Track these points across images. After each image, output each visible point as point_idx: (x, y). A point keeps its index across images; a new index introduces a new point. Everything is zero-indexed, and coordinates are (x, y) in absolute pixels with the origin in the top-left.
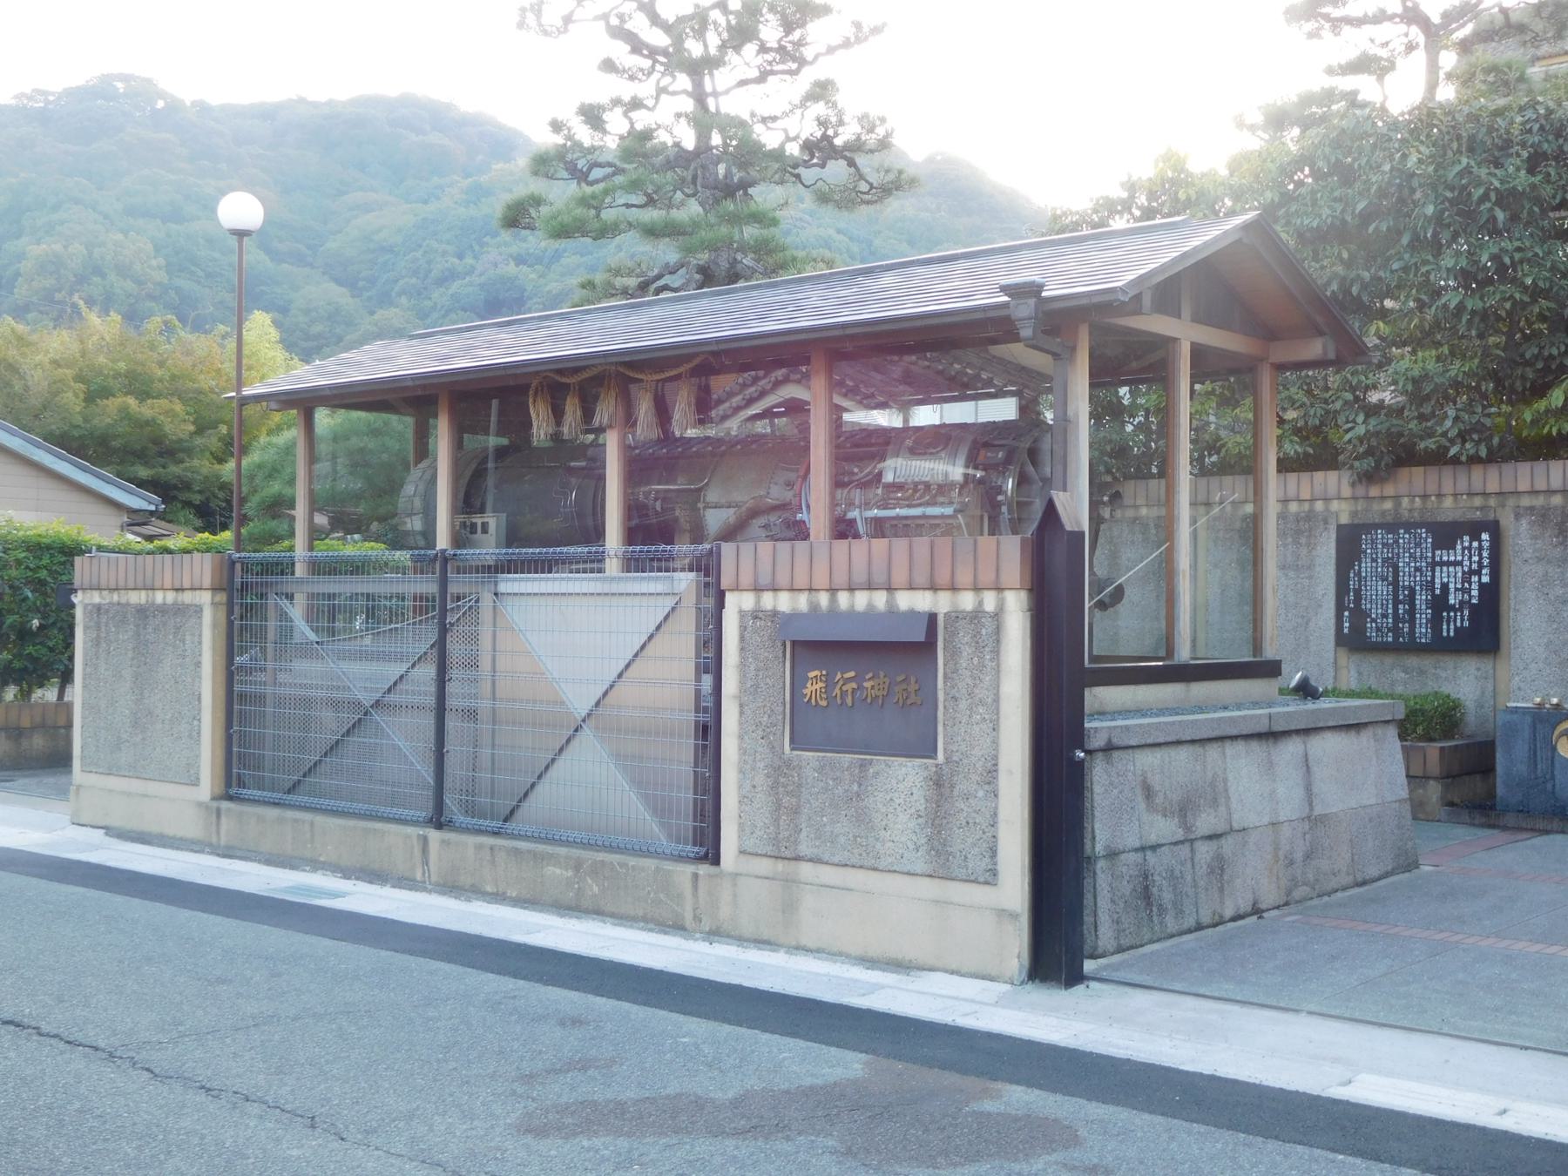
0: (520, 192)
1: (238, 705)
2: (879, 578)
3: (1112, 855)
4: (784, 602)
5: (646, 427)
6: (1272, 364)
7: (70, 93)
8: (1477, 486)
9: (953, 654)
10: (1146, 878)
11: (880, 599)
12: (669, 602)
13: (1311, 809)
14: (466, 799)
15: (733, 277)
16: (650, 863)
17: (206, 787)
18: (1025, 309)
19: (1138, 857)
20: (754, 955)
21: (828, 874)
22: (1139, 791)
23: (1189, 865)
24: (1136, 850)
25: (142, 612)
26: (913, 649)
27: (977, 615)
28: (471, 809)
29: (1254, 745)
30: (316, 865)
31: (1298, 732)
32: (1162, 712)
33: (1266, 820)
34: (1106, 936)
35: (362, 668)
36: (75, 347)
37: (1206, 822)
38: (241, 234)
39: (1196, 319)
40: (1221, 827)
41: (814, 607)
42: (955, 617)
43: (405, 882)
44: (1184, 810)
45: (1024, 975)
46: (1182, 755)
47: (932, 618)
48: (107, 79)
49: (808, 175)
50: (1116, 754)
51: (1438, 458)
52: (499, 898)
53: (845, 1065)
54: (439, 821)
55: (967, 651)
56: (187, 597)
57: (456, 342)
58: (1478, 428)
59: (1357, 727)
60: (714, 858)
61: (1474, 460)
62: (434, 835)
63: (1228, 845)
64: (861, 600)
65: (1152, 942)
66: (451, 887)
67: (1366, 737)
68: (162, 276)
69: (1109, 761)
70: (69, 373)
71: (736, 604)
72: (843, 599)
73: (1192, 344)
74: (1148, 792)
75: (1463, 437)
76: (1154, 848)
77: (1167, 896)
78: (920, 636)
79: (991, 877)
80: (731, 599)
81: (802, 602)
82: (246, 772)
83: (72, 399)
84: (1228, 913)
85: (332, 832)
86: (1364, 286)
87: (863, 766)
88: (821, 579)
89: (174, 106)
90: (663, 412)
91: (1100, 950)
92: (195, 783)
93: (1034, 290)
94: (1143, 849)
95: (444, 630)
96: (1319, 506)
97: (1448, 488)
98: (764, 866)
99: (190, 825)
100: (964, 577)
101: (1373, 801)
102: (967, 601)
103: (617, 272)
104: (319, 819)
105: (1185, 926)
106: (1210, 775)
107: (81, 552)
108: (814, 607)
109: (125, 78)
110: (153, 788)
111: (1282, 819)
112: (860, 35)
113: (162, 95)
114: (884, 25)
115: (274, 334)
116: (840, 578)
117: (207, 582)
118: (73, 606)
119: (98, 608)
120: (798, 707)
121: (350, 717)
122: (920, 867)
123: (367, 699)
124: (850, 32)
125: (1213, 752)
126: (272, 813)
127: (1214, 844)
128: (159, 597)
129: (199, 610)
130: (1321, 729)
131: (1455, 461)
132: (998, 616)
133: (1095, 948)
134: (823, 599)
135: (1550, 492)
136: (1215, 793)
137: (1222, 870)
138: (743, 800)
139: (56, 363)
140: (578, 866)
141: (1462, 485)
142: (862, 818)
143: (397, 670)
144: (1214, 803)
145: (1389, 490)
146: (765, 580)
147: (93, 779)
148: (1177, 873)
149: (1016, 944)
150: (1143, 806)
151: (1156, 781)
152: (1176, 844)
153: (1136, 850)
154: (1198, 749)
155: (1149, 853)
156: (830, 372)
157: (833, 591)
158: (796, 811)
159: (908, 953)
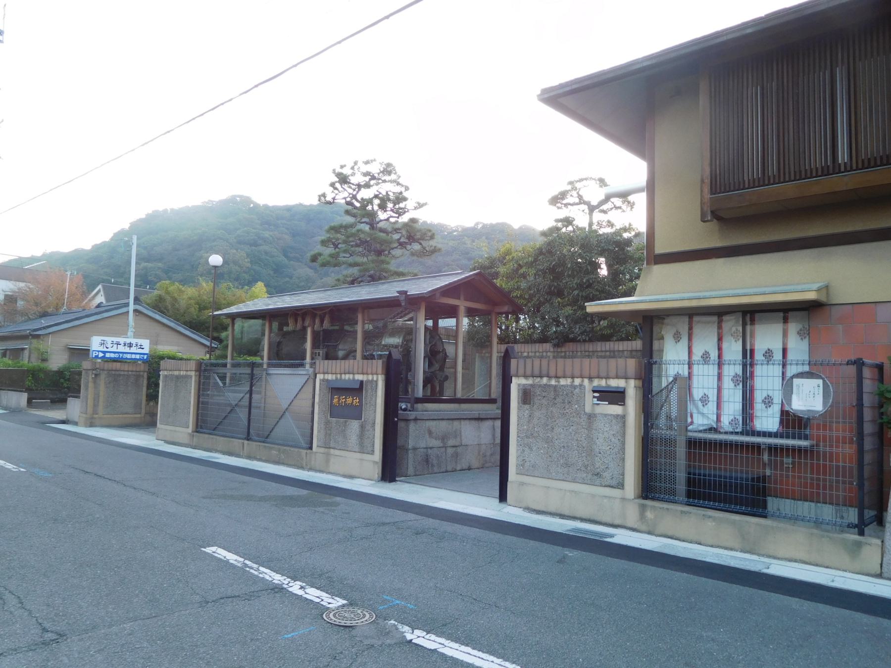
0: (316, 251)
1: (201, 405)
2: (603, 374)
3: (415, 449)
4: (330, 377)
5: (317, 326)
7: (221, 201)
8: (587, 349)
9: (367, 391)
11: (351, 376)
12: (307, 377)
14: (255, 431)
15: (380, 279)
16: (296, 450)
17: (190, 430)
18: (402, 298)
20: (311, 473)
21: (337, 452)
25: (178, 377)
26: (358, 390)
27: (372, 380)
28: (258, 435)
29: (473, 422)
30: (216, 451)
31: (491, 419)
34: (411, 470)
35: (234, 395)
36: (197, 293)
37: (451, 442)
38: (215, 267)
39: (466, 300)
41: (337, 378)
42: (368, 381)
43: (238, 456)
44: (444, 438)
46: (444, 423)
47: (362, 382)
48: (234, 197)
49: (409, 247)
51: (574, 340)
52: (260, 460)
53: (304, 492)
54: (248, 438)
55: (370, 391)
56: (189, 373)
57: (321, 295)
58: (585, 331)
60: (311, 448)
61: (585, 341)
62: (246, 442)
63: (459, 450)
64: (347, 377)
66: (249, 457)
68: (249, 265)
70: (192, 302)
71: (320, 377)
72: (343, 376)
74: (430, 433)
75: (582, 333)
76: (431, 448)
77: (435, 462)
78: (358, 387)
79: (372, 452)
81: (334, 377)
82: (201, 426)
83: (194, 311)
84: (458, 468)
85: (221, 441)
86: (555, 287)
87: (346, 422)
88: (338, 371)
89: (257, 206)
90: (322, 322)
92: (188, 427)
93: (405, 292)
95: (251, 386)
96: (545, 354)
97: (579, 349)
98: (322, 450)
99: (186, 440)
100: (369, 371)
102: (370, 377)
103: (347, 276)
104: (218, 438)
108: (337, 378)
109: (239, 196)
110: (178, 429)
112: (420, 206)
113: (252, 202)
114: (426, 204)
115: (265, 289)
116: (342, 371)
118: (159, 375)
119: (166, 376)
120: (332, 405)
121: (229, 409)
122: (357, 450)
123: (234, 403)
124: (416, 205)
125: (456, 423)
126: (207, 436)
127: (454, 449)
128: (182, 373)
129: (191, 377)
131: (579, 341)
132: (376, 382)
134: (339, 376)
135: (606, 351)
136: (457, 434)
138: (319, 432)
139: (190, 298)
140: (279, 450)
141: (583, 349)
142: (345, 437)
143: (242, 395)
144: (456, 437)
145: (563, 350)
146: (593, 374)
147: (163, 426)
149: (377, 471)
151: (433, 430)
154: (451, 422)
156: (363, 313)
157: (341, 374)
158: (330, 435)
159: (354, 473)
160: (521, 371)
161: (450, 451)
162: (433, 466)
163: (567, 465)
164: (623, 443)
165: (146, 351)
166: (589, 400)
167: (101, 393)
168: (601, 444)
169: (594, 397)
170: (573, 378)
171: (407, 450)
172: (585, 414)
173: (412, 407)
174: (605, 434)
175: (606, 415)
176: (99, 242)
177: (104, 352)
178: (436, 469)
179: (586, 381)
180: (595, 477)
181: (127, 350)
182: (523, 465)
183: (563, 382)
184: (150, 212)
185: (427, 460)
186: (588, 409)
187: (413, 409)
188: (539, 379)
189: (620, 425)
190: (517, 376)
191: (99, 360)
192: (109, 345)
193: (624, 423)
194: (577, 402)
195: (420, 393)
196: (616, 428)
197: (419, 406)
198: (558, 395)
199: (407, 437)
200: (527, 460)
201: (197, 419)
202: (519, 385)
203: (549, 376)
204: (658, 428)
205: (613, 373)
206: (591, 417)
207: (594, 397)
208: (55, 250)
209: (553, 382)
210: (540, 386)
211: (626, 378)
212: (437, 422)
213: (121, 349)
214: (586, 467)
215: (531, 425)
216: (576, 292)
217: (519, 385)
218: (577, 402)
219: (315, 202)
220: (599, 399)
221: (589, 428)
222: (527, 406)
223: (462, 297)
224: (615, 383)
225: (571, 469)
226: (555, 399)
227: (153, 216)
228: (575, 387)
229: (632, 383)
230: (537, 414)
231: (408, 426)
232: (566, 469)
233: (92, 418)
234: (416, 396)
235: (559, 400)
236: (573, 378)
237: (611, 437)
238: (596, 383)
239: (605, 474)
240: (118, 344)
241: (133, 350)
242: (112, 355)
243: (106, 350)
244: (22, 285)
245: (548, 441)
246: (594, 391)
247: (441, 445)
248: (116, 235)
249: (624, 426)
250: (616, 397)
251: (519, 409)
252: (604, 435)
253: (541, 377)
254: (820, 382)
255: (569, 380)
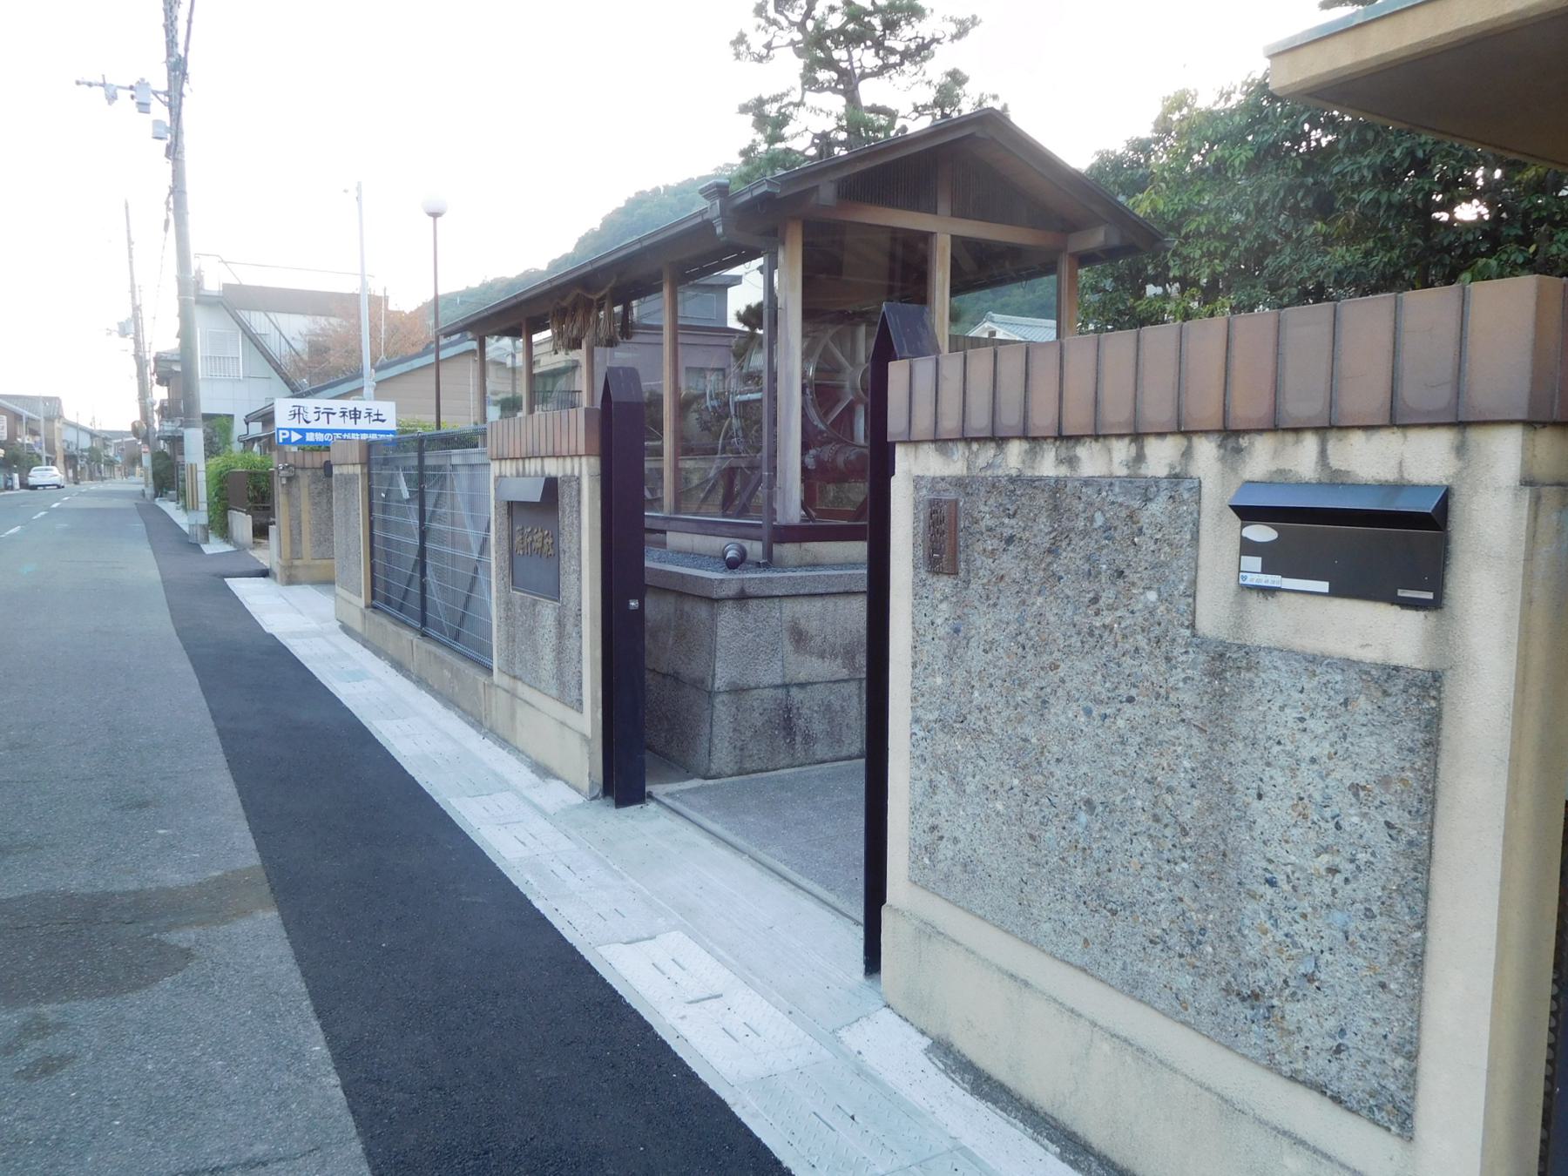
2: (1304, 404)
3: (737, 690)
6: (1073, 255)
22: (785, 636)
32: (841, 566)
34: (723, 756)
39: (960, 213)
45: (598, 790)
50: (753, 604)
73: (953, 237)
74: (799, 637)
76: (802, 685)
77: (818, 727)
80: (904, 462)
86: (1308, 191)
87: (534, 603)
91: (712, 773)
94: (786, 686)
112: (963, 29)
114: (974, 21)
117: (582, 450)
133: (709, 770)
146: (1248, 408)
151: (812, 626)
160: (923, 423)
162: (809, 739)
163: (1099, 899)
164: (1421, 856)
165: (390, 425)
166: (1221, 558)
167: (305, 517)
168: (1276, 833)
169: (1248, 547)
170: (1137, 436)
171: (711, 694)
172: (1197, 641)
173: (768, 553)
174: (1306, 773)
175: (1314, 661)
176: (557, 256)
177: (302, 432)
178: (820, 750)
179: (1206, 451)
180: (1241, 1010)
181: (349, 424)
182: (930, 850)
183: (1093, 461)
184: (632, 195)
185: (786, 723)
186: (1213, 616)
187: (769, 562)
188: (990, 451)
189: (1408, 732)
190: (910, 442)
191: (294, 449)
192: (311, 416)
193: (1433, 724)
194: (1158, 574)
195: (791, 509)
196: (1380, 749)
197: (788, 551)
198: (1066, 534)
199: (712, 653)
200: (946, 829)
201: (373, 578)
202: (917, 481)
203: (1034, 440)
204: (1480, 216)
205: (1366, 396)
206: (1227, 663)
207: (1248, 547)
208: (499, 276)
209: (1048, 466)
210: (994, 485)
211: (1461, 422)
212: (830, 603)
213: (337, 423)
214: (1195, 939)
215: (959, 676)
216: (1367, 196)
217: (917, 481)
218: (1158, 574)
220: (1274, 560)
221: (1217, 722)
222: (944, 584)
223: (944, 206)
224: (1378, 461)
225: (1119, 927)
226: (1053, 551)
227: (638, 202)
228: (1146, 490)
229: (1504, 453)
230: (981, 622)
231: (713, 618)
232: (1099, 921)
233: (291, 567)
234: (781, 520)
235: (1071, 558)
236: (1137, 436)
237: (1343, 802)
238: (1262, 458)
239: (1295, 1012)
240: (329, 413)
241: (363, 424)
242: (320, 437)
243: (303, 425)
244: (322, 321)
245: (1026, 759)
246: (1247, 514)
248: (582, 241)
249: (1432, 745)
250: (1394, 549)
251: (919, 586)
252: (1301, 780)
253: (998, 439)
255: (1122, 450)
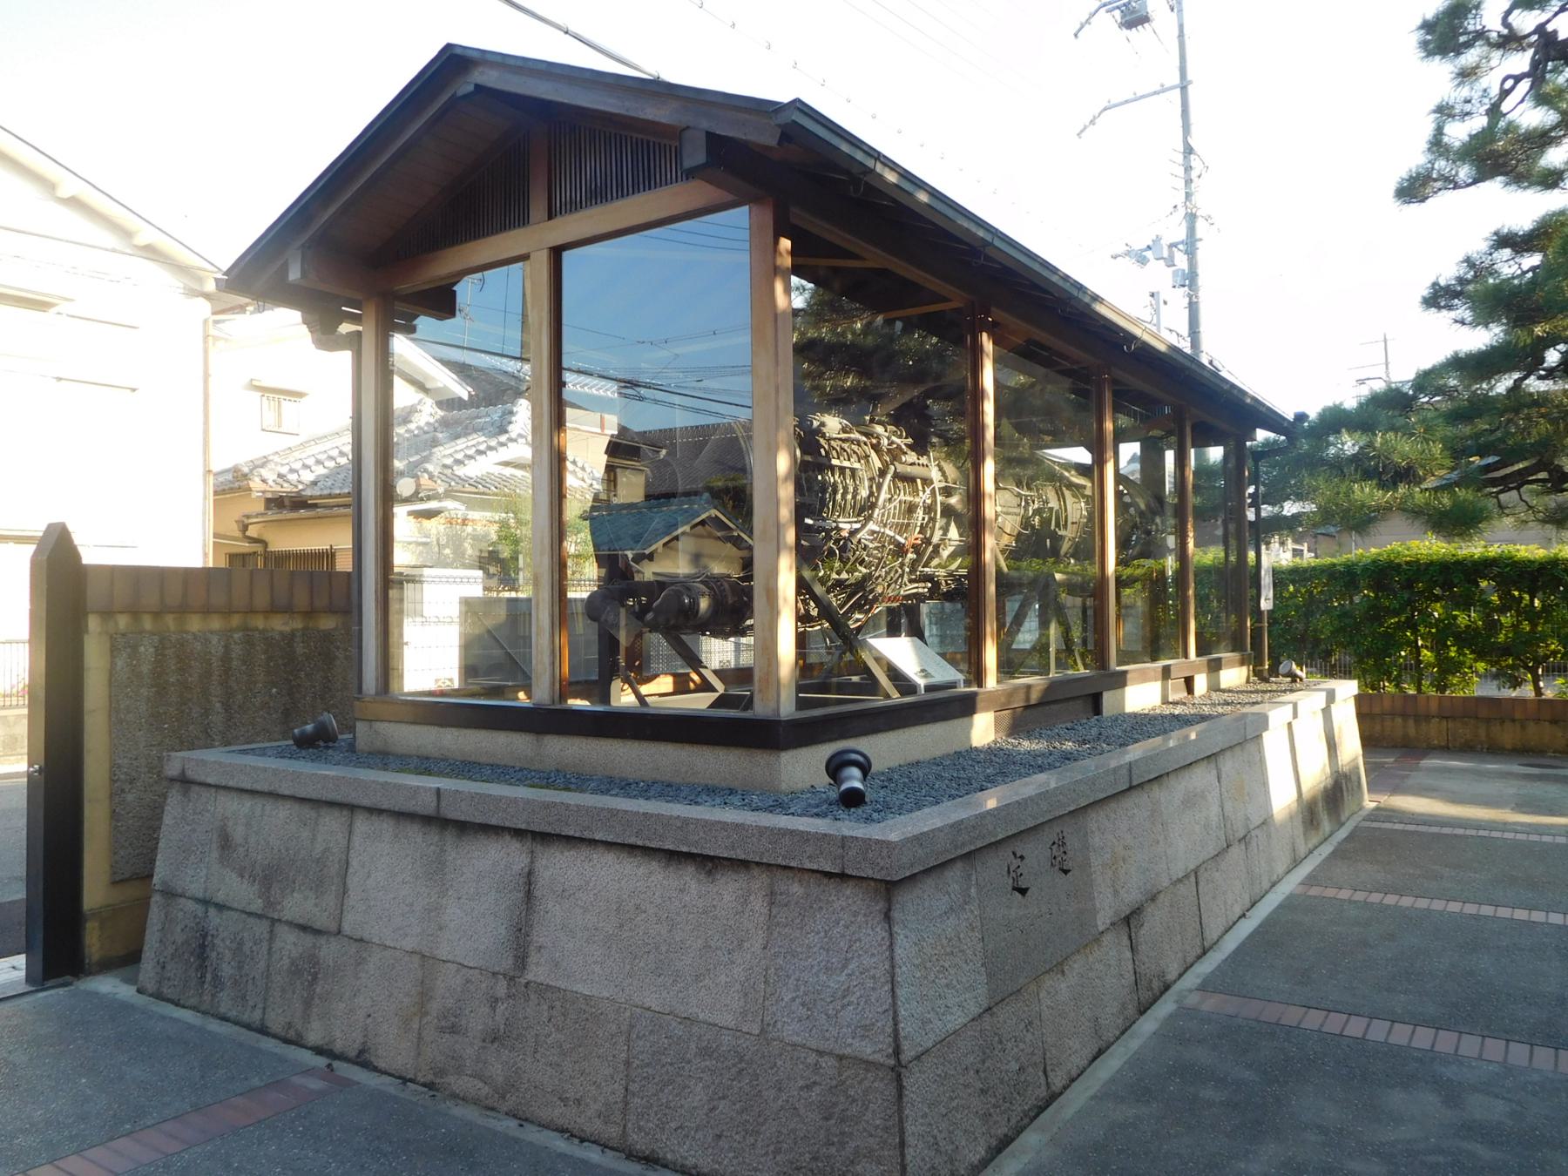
10: (204, 937)
13: (521, 961)
19: (200, 909)
23: (265, 945)
24: (198, 900)
29: (414, 832)
33: (409, 944)
37: (298, 905)
40: (322, 920)
44: (270, 878)
46: (282, 813)
59: (709, 864)
63: (329, 950)
65: (194, 1008)
67: (728, 888)
69: (185, 793)
74: (226, 843)
76: (221, 907)
77: (227, 970)
84: (314, 1036)
94: (206, 902)
101: (728, 1020)
105: (245, 1017)
106: (319, 848)
107: (413, 581)
111: (443, 952)
122: (1305, 789)
125: (332, 823)
127: (308, 940)
130: (593, 842)
136: (333, 877)
137: (315, 978)
148: (246, 949)
150: (215, 854)
151: (238, 833)
152: (250, 914)
153: (198, 900)
154: (308, 812)
155: (212, 911)
161: (290, 943)
162: (217, 982)
185: (201, 949)
212: (258, 804)
219: (1291, 417)
247: (257, 905)
254: (456, 685)
